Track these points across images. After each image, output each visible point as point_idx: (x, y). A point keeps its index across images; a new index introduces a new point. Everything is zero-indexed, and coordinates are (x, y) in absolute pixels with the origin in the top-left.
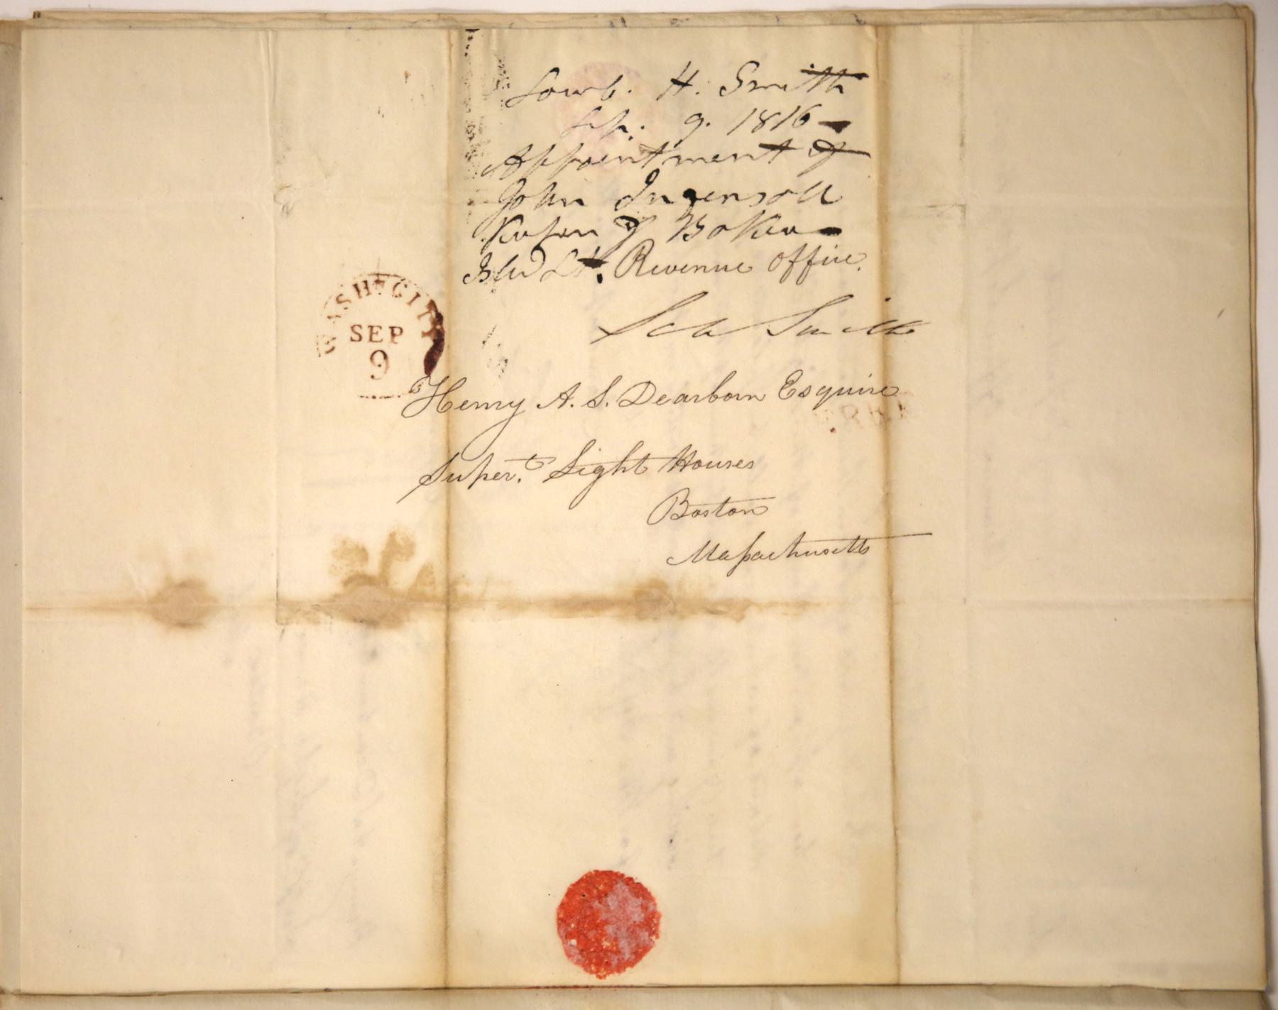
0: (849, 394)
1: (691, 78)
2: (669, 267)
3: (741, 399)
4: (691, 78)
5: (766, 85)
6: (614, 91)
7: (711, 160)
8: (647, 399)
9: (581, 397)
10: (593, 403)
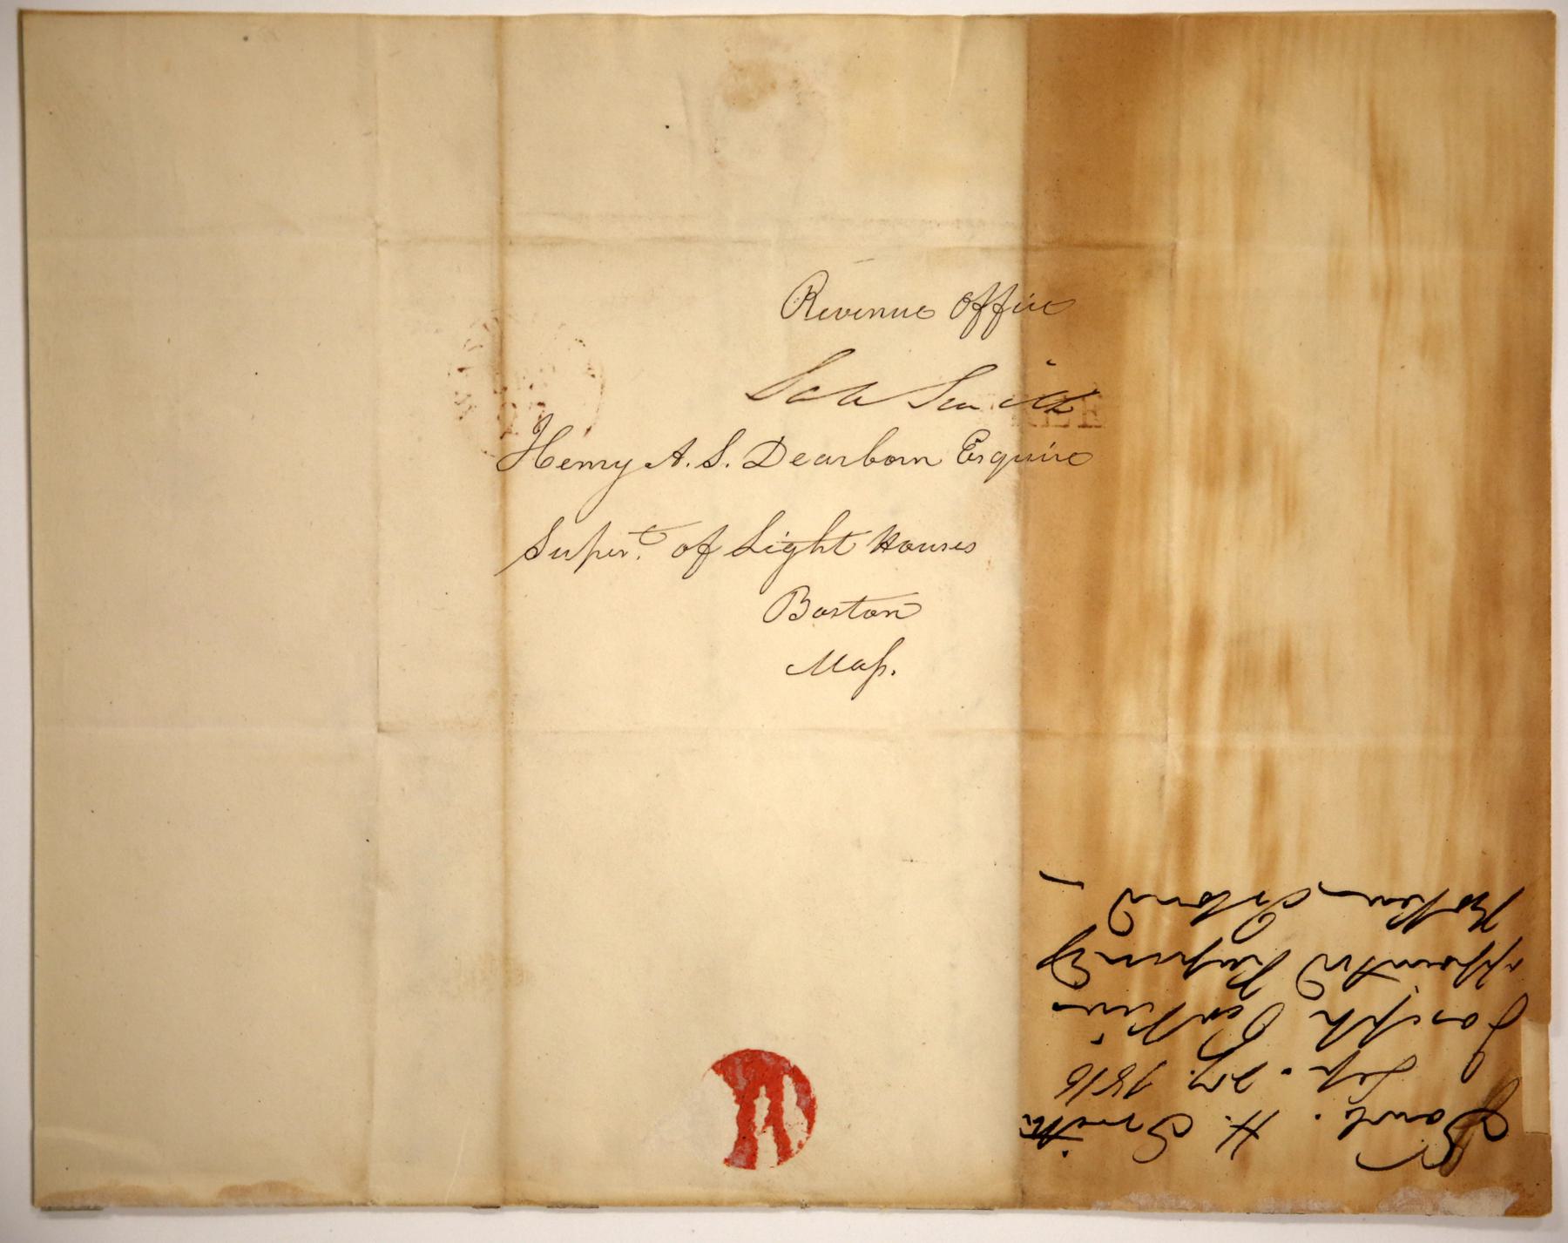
5: (497, 430)
9: (695, 456)
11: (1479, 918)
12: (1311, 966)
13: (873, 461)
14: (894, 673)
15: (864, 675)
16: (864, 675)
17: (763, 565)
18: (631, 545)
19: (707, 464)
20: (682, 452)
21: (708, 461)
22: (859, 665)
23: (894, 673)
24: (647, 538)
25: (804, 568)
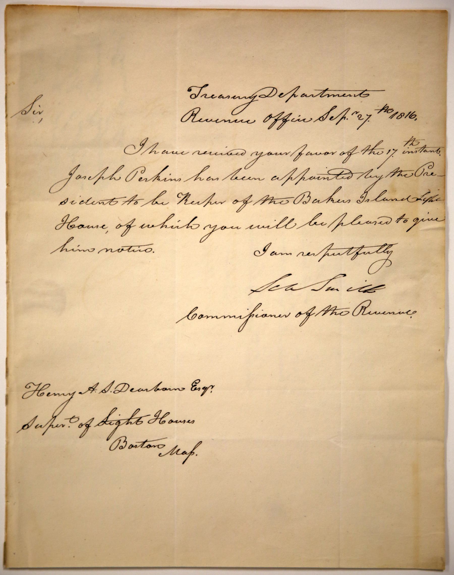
0: (276, 155)
1: (388, 258)
2: (120, 249)
3: (145, 179)
4: (388, 258)
5: (176, 389)
6: (137, 172)
7: (441, 148)
8: (125, 390)
9: (99, 388)
10: (104, 391)
11: (338, 177)
12: (417, 172)
13: (158, 389)
14: (197, 455)
15: (187, 456)
16: (187, 456)
17: (108, 429)
18: (67, 423)
19: (104, 391)
20: (94, 388)
21: (104, 390)
22: (184, 453)
23: (197, 455)
24: (73, 420)
25: (123, 430)
